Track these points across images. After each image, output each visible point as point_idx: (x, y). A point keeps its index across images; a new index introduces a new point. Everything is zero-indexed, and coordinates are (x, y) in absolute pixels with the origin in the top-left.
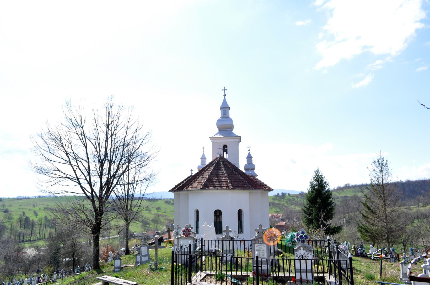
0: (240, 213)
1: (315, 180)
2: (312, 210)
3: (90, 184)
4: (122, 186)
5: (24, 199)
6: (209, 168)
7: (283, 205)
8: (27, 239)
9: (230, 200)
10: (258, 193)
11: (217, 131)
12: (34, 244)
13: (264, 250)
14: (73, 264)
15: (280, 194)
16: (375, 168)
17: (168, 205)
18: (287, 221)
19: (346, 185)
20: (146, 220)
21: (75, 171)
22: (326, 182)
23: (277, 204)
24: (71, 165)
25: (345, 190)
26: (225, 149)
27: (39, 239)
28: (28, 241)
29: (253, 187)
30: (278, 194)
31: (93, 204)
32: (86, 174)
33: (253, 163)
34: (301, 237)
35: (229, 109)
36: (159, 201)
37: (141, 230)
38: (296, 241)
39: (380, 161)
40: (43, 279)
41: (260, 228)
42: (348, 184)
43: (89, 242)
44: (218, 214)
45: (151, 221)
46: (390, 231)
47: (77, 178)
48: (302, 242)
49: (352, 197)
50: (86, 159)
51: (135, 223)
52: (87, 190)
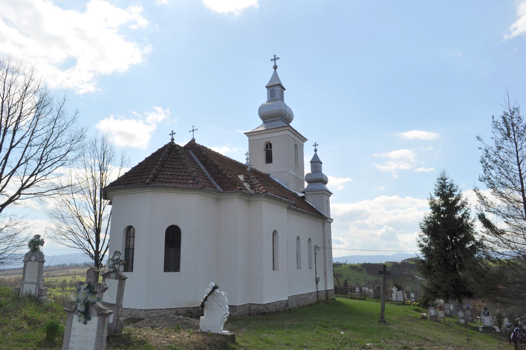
33: (324, 171)
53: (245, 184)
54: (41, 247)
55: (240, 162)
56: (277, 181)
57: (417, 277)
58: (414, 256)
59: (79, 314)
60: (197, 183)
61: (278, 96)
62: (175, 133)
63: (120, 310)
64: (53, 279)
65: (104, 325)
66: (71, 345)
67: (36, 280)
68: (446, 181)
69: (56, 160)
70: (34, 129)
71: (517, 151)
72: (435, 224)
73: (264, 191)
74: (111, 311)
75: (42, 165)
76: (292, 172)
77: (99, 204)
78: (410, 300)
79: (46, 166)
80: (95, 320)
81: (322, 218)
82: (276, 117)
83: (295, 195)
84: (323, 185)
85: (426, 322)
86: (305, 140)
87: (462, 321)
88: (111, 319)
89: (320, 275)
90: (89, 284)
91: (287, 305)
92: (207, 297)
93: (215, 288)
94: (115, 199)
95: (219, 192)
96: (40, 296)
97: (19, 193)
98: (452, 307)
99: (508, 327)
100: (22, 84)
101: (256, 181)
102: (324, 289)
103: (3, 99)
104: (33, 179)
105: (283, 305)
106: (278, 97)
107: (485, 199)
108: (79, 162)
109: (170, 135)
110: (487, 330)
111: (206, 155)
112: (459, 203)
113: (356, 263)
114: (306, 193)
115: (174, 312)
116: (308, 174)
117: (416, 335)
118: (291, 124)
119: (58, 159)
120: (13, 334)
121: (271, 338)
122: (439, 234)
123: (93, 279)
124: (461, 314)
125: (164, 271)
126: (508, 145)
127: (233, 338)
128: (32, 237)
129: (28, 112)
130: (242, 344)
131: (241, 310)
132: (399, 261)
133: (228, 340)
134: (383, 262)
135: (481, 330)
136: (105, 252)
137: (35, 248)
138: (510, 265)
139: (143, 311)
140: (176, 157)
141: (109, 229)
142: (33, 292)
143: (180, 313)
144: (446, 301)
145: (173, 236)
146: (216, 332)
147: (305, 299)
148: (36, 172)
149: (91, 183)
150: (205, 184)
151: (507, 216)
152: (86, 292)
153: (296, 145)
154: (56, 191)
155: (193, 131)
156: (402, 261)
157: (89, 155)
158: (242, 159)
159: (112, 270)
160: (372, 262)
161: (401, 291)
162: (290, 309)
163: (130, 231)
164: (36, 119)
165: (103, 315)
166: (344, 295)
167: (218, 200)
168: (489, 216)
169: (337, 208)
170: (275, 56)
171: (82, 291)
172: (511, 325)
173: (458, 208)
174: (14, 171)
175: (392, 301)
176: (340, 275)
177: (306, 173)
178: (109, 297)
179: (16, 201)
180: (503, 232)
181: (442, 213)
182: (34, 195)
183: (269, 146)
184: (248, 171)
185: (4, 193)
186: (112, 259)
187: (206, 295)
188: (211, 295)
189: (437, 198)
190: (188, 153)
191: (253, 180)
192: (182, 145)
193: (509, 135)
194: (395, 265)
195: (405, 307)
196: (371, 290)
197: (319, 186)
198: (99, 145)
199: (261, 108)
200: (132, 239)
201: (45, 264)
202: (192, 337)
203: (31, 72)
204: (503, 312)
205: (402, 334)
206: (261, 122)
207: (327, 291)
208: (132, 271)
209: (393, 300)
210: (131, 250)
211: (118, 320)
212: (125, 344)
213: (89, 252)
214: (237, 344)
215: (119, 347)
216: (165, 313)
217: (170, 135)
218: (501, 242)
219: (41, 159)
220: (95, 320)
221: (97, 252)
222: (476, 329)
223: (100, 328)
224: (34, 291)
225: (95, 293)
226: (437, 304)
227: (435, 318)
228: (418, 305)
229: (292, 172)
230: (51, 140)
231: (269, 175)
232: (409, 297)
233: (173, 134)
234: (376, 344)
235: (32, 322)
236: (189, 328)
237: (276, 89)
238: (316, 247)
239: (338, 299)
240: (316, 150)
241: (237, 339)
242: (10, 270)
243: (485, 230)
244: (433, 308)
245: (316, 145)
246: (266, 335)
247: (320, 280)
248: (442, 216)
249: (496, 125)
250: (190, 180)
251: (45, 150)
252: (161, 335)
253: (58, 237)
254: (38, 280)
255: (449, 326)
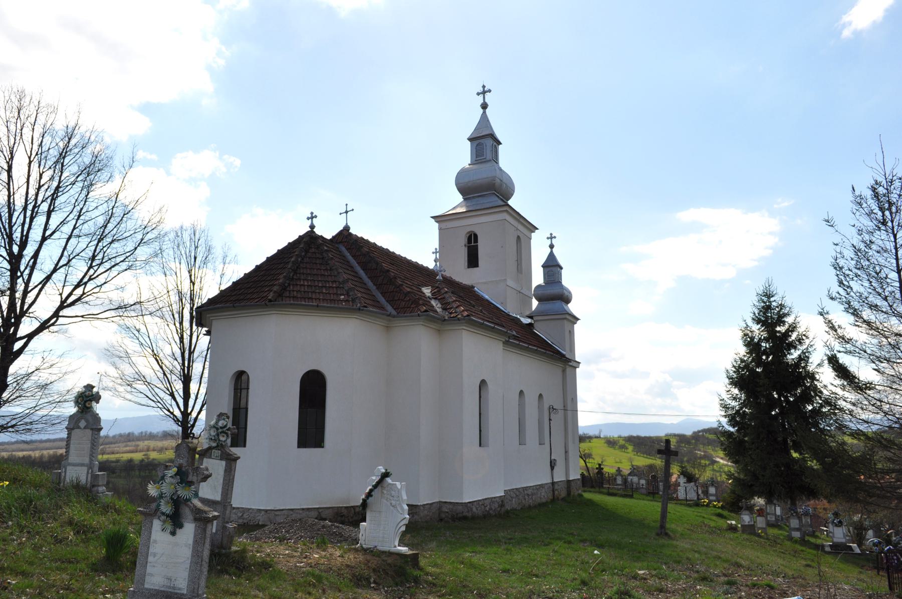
17: (611, 450)
33: (565, 282)
36: (594, 440)
53: (433, 302)
54: (94, 404)
55: (425, 265)
56: (487, 297)
57: (718, 459)
58: (715, 425)
59: (163, 518)
60: (353, 300)
61: (489, 155)
62: (316, 217)
63: (228, 512)
64: (112, 457)
65: (205, 538)
66: (149, 569)
67: (87, 460)
68: (772, 299)
69: (118, 260)
70: (82, 209)
71: (896, 249)
72: (752, 372)
73: (466, 313)
74: (216, 514)
75: (95, 268)
76: (510, 283)
77: (189, 333)
78: (707, 498)
79: (101, 270)
80: (189, 530)
81: (561, 360)
82: (484, 189)
83: (516, 321)
84: (564, 304)
85: (736, 535)
86: (533, 228)
87: (797, 535)
88: (214, 527)
89: (558, 455)
90: (180, 468)
91: (502, 505)
92: (371, 491)
93: (386, 475)
94: (217, 325)
95: (389, 315)
96: (93, 486)
97: (56, 315)
98: (778, 511)
99: (875, 545)
100: (61, 133)
101: (451, 298)
102: (564, 479)
103: (30, 158)
104: (79, 291)
105: (496, 505)
106: (489, 157)
107: (839, 331)
108: (155, 267)
109: (308, 219)
110: (838, 549)
111: (368, 253)
112: (794, 336)
113: (616, 436)
114: (535, 318)
115: (315, 514)
116: (539, 287)
117: (720, 558)
118: (510, 202)
119: (122, 259)
120: (50, 549)
121: (477, 559)
122: (759, 389)
123: (186, 459)
124: (794, 523)
125: (299, 447)
126: (882, 238)
127: (414, 559)
128: (79, 388)
129: (72, 180)
130: (430, 569)
131: (426, 512)
132: (689, 433)
133: (407, 562)
134: (661, 433)
135: (828, 549)
136: (199, 413)
137: (85, 406)
138: (878, 441)
139: (263, 513)
140: (318, 255)
141: (206, 374)
142: (83, 479)
143: (324, 516)
144: (769, 501)
145: (313, 389)
146: (386, 549)
147: (532, 494)
148: (85, 280)
149: (174, 298)
150: (367, 301)
151: (879, 359)
152: (174, 481)
153: (518, 237)
154: (113, 313)
155: (347, 212)
156: (694, 433)
157: (171, 253)
158: (429, 262)
159: (214, 445)
160: (643, 434)
161: (692, 484)
162: (507, 512)
163: (241, 380)
164: (84, 192)
165: (202, 520)
166: (597, 489)
167: (388, 328)
168: (844, 359)
169: (585, 342)
170: (484, 87)
171: (168, 480)
172: (880, 543)
173: (792, 346)
174: (48, 278)
175: (677, 499)
176: (589, 456)
177: (535, 284)
178: (210, 490)
179: (51, 328)
180: (869, 386)
181: (765, 352)
182: (81, 319)
183: (472, 240)
184: (438, 280)
185: (31, 315)
186: (214, 427)
187: (370, 487)
188: (379, 488)
189: (756, 328)
190: (337, 249)
191: (447, 296)
192: (328, 236)
193: (884, 223)
194: (682, 438)
195: (700, 509)
196: (643, 482)
197: (558, 304)
198: (186, 237)
199: (461, 175)
200: (244, 392)
201: (102, 433)
202: (346, 556)
203: (77, 114)
204: (865, 519)
205: (697, 555)
206: (459, 198)
207: (569, 482)
208: (245, 446)
209: (680, 498)
210: (243, 411)
211: (224, 528)
212: (237, 568)
213: (172, 413)
214: (421, 569)
215: (227, 573)
216: (299, 516)
217: (308, 219)
218: (866, 402)
219: (93, 258)
220: (189, 530)
221: (186, 414)
222: (818, 547)
223: (198, 541)
224: (85, 478)
225: (190, 483)
226: (754, 505)
227: (750, 529)
228: (722, 507)
229: (510, 283)
230: (110, 226)
231: (473, 287)
232: (706, 493)
233: (312, 217)
234: (654, 572)
235: (81, 529)
236: (340, 542)
237: (484, 142)
238: (552, 409)
239: (587, 495)
240: (552, 246)
241: (422, 562)
242: (41, 441)
243: (838, 382)
244: (747, 512)
245: (551, 237)
246: (468, 554)
247: (558, 463)
248: (764, 357)
249: (859, 202)
250: (341, 295)
251: (100, 244)
252: (295, 554)
253: (121, 389)
254: (91, 460)
255: (774, 542)
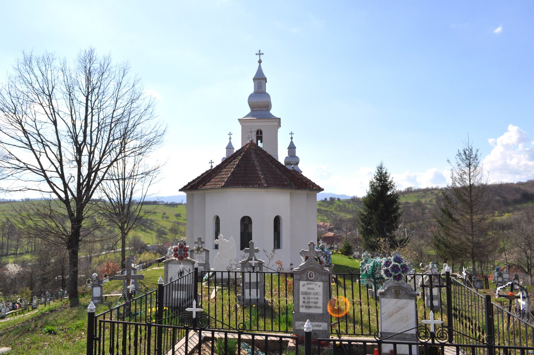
0: (277, 221)
1: (377, 179)
2: (371, 218)
3: (62, 176)
4: (116, 182)
5: (8, 202)
6: (235, 159)
7: (331, 212)
8: (13, 252)
9: (264, 204)
10: (302, 194)
11: (248, 110)
12: (21, 258)
13: (317, 294)
14: (62, 285)
15: (328, 199)
16: (460, 162)
18: (335, 231)
19: (408, 189)
20: (162, 229)
21: (38, 159)
22: (391, 182)
23: (325, 211)
24: (33, 150)
25: (406, 195)
26: (259, 135)
27: (27, 252)
28: (13, 254)
29: (296, 185)
30: (326, 199)
31: (67, 206)
32: (57, 165)
34: (395, 268)
35: (266, 82)
37: (156, 241)
38: (384, 276)
39: (467, 152)
40: (20, 305)
41: (310, 250)
42: (410, 188)
43: (89, 256)
44: (246, 223)
45: (169, 230)
46: (478, 245)
47: (42, 168)
48: (395, 277)
49: (414, 203)
50: (56, 142)
51: (148, 232)
52: (57, 187)
